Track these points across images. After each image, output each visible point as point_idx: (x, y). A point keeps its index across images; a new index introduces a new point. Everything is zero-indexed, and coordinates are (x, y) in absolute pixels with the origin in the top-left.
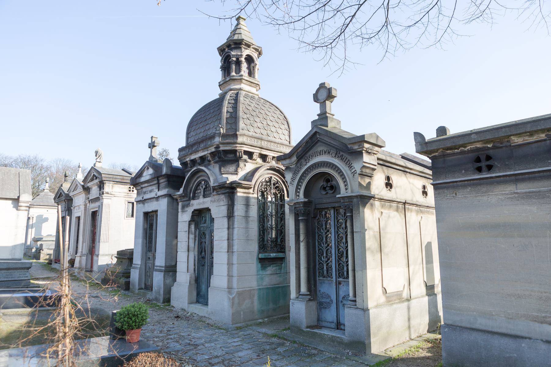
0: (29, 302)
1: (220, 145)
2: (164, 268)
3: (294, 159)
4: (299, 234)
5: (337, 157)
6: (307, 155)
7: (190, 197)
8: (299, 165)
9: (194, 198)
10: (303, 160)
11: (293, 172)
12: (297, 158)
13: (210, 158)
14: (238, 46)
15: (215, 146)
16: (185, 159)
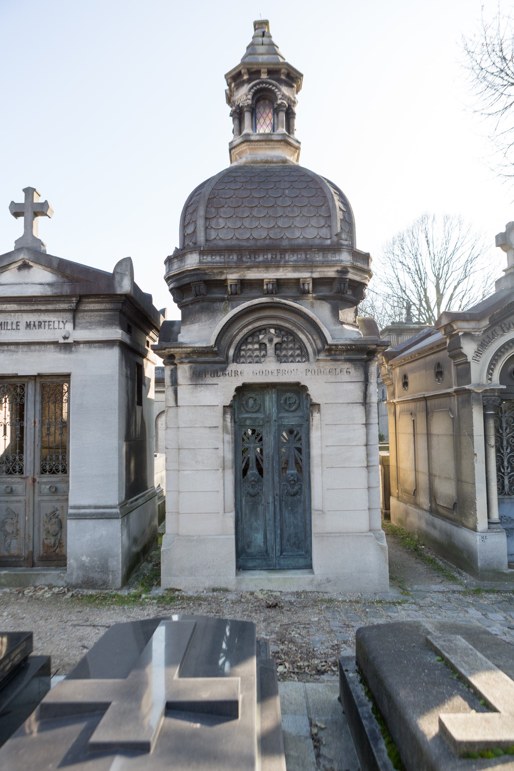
0: (38, 648)
1: (350, 270)
2: (117, 510)
3: (486, 323)
4: (141, 428)
5: (506, 330)
6: (506, 321)
7: (227, 357)
8: (489, 333)
9: (237, 358)
10: (497, 328)
11: (479, 343)
12: (490, 322)
13: (309, 287)
14: (290, 82)
15: (339, 268)
16: (222, 273)
